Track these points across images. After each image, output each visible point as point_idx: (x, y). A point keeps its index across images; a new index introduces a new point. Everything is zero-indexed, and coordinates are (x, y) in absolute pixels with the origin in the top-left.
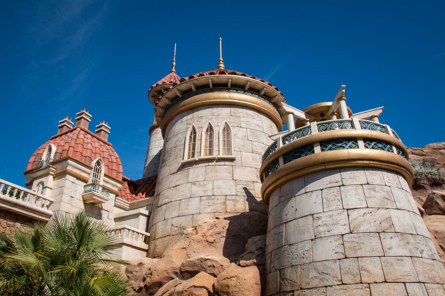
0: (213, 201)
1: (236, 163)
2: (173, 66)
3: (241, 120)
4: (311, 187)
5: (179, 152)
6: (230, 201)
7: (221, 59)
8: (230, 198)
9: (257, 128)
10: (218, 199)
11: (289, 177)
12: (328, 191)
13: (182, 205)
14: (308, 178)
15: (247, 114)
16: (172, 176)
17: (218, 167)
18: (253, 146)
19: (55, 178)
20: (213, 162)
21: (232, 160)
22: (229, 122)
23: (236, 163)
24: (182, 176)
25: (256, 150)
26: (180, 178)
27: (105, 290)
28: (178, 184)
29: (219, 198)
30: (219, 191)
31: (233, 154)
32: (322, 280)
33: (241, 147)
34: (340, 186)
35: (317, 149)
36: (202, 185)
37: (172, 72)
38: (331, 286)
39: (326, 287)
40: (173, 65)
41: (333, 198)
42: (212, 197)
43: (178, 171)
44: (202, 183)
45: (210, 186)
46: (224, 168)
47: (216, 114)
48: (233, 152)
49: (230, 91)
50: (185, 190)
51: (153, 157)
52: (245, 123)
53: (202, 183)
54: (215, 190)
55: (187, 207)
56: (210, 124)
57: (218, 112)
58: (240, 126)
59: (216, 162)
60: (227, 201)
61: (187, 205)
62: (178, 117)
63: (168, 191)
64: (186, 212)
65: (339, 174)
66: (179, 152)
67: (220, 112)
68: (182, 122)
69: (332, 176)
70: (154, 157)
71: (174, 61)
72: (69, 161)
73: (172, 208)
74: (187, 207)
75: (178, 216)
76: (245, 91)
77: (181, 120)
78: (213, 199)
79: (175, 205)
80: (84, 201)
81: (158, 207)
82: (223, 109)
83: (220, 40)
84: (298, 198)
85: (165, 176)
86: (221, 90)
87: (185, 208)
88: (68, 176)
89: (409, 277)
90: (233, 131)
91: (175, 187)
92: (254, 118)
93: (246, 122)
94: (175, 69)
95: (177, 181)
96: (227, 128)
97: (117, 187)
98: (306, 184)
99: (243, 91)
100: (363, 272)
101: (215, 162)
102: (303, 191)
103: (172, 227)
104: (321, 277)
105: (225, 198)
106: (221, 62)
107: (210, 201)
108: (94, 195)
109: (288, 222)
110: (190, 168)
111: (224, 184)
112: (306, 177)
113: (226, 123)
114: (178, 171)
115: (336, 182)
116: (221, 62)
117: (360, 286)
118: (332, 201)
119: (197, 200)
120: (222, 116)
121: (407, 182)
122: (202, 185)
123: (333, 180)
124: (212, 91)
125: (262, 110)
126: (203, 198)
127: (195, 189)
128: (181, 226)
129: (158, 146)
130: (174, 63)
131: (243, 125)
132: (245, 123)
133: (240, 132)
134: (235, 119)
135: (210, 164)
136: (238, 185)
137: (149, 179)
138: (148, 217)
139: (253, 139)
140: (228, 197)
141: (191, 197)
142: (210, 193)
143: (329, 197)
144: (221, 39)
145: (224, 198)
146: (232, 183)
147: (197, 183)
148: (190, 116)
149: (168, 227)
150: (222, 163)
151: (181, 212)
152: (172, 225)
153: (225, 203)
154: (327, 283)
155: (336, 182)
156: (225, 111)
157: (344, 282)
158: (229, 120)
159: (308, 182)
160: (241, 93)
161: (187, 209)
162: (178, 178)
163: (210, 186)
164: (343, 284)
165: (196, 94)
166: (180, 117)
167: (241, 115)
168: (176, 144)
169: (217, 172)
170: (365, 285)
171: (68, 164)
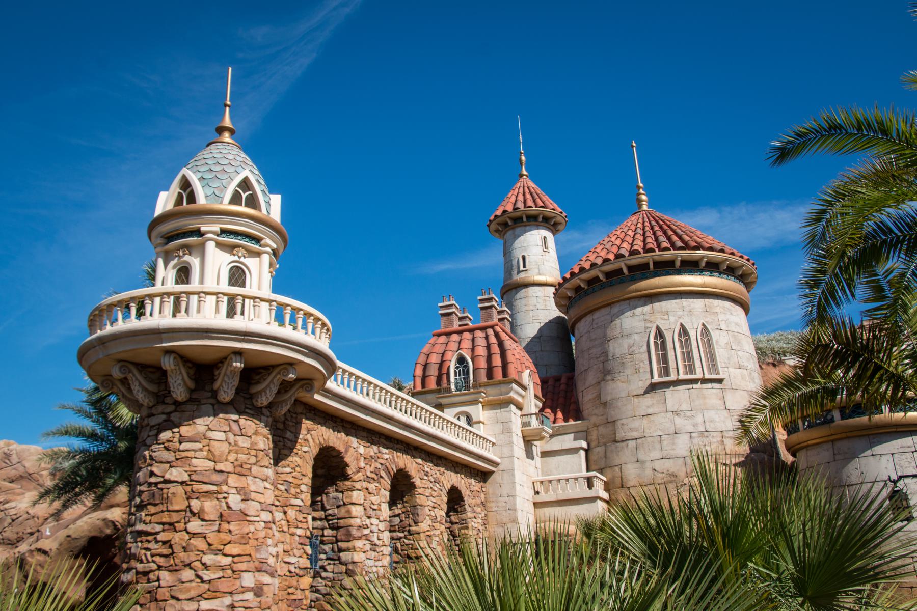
0: (708, 439)
1: (725, 385)
2: (521, 164)
4: (878, 449)
5: (642, 364)
6: (728, 439)
7: (641, 185)
8: (727, 435)
10: (713, 436)
11: (849, 434)
12: (900, 456)
13: (665, 443)
14: (874, 438)
15: (724, 307)
16: (636, 400)
17: (704, 391)
18: (739, 358)
19: (485, 407)
20: (697, 383)
21: (720, 381)
22: (706, 322)
23: (725, 385)
24: (655, 402)
26: (653, 404)
28: (650, 411)
29: (715, 435)
30: (712, 425)
31: (721, 372)
33: (726, 361)
34: (913, 452)
35: (886, 409)
36: (689, 417)
37: (521, 176)
40: (521, 160)
41: (907, 465)
42: (706, 434)
43: (646, 392)
44: (688, 414)
45: (699, 419)
46: (711, 392)
47: (687, 309)
48: (720, 369)
49: (703, 273)
50: (663, 422)
51: (529, 340)
52: (724, 322)
53: (688, 414)
55: (674, 447)
56: (682, 325)
57: (689, 306)
58: (719, 327)
59: (701, 384)
60: (724, 440)
61: (674, 444)
62: (624, 305)
63: (634, 420)
64: (673, 453)
65: (910, 438)
66: (642, 364)
67: (692, 305)
68: (634, 315)
69: (903, 439)
70: (531, 340)
71: (521, 153)
72: (514, 386)
73: (648, 445)
74: (674, 447)
76: (720, 273)
77: (632, 311)
78: (707, 437)
79: (653, 442)
80: (524, 437)
81: (615, 441)
82: (695, 300)
83: (633, 146)
84: (863, 460)
85: (620, 396)
86: (691, 272)
87: (670, 448)
88: (512, 406)
90: (715, 335)
91: (645, 417)
92: (732, 314)
94: (527, 170)
95: (648, 407)
96: (705, 331)
97: (890, 515)
98: (871, 445)
99: (718, 272)
101: (699, 383)
102: (868, 452)
103: (656, 473)
105: (721, 435)
106: (641, 191)
107: (704, 439)
108: (544, 430)
109: (852, 485)
110: (665, 390)
111: (717, 416)
112: (871, 437)
113: (703, 325)
114: (646, 392)
115: (909, 447)
116: (641, 191)
118: (906, 468)
119: (686, 437)
120: (695, 313)
121: (744, 310)
122: (689, 417)
123: (904, 444)
124: (678, 272)
125: (739, 300)
126: (693, 435)
127: (679, 421)
128: (670, 472)
129: (535, 321)
130: (523, 158)
131: (723, 327)
133: (722, 337)
134: (713, 317)
135: (694, 386)
136: (732, 416)
138: (587, 451)
139: (738, 348)
141: (676, 433)
142: (702, 429)
143: (902, 463)
144: (634, 144)
146: (725, 413)
147: (680, 413)
148: (647, 308)
149: (646, 472)
150: (709, 385)
152: (655, 470)
153: (723, 441)
155: (909, 447)
156: (698, 304)
158: (706, 320)
159: (874, 443)
160: (716, 277)
161: (673, 449)
162: (649, 402)
163: (699, 419)
165: (656, 275)
166: (628, 306)
167: (718, 310)
168: (631, 350)
169: (705, 398)
171: (512, 389)
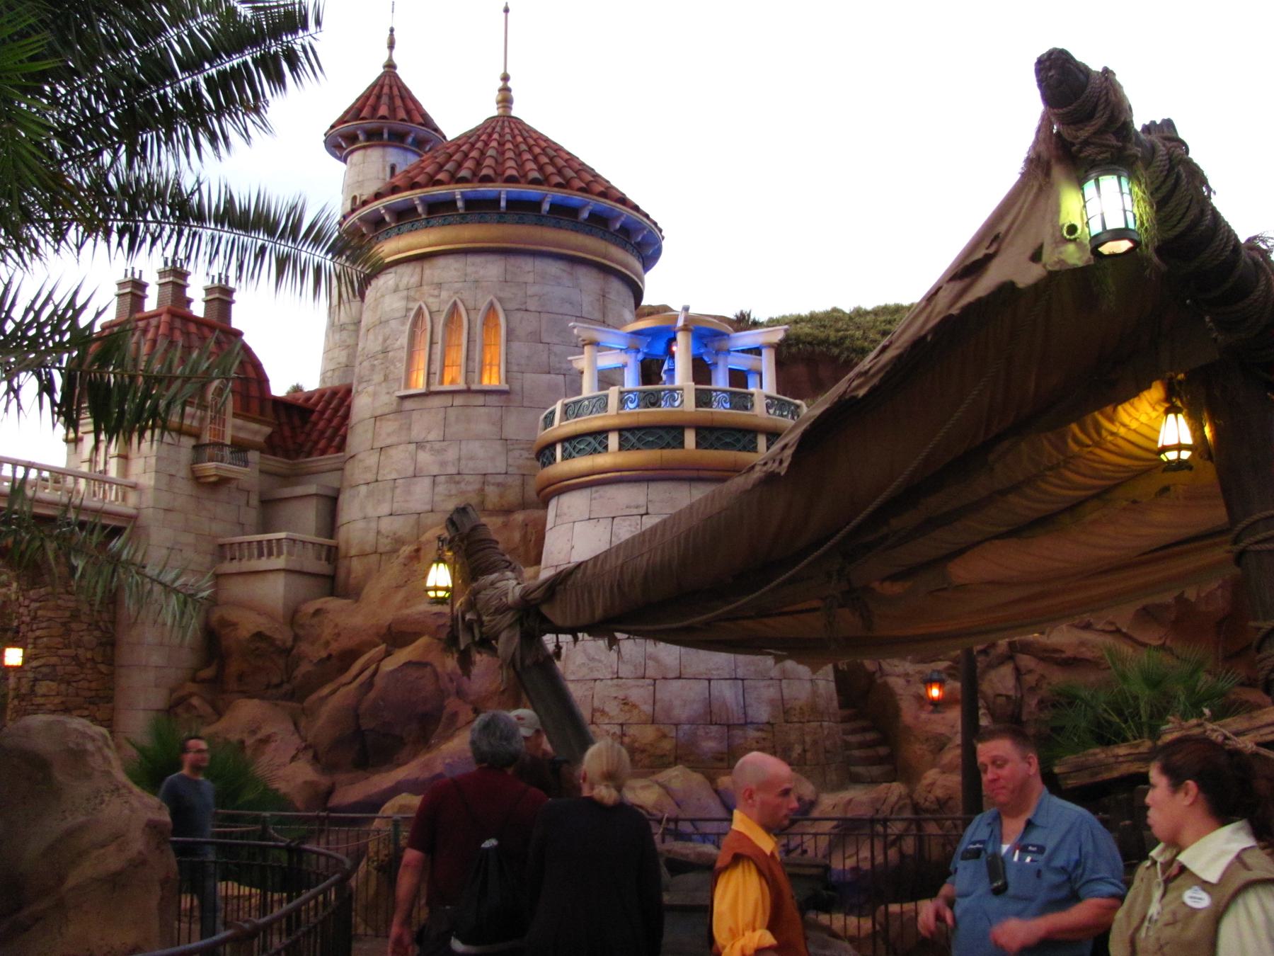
3: (529, 293)
9: (567, 308)
14: (597, 491)
25: (558, 366)
27: (33, 154)
28: (389, 442)
30: (471, 464)
32: (591, 670)
34: (642, 515)
38: (602, 680)
39: (595, 680)
42: (457, 478)
54: (463, 462)
57: (476, 272)
60: (486, 487)
75: (391, 515)
89: (720, 672)
92: (559, 284)
93: (540, 297)
100: (650, 663)
104: (592, 665)
117: (641, 682)
119: (427, 482)
131: (532, 305)
132: (537, 298)
137: (334, 393)
140: (490, 478)
145: (479, 478)
151: (395, 505)
154: (596, 675)
157: (620, 675)
164: (618, 678)
167: (530, 278)
170: (648, 681)
